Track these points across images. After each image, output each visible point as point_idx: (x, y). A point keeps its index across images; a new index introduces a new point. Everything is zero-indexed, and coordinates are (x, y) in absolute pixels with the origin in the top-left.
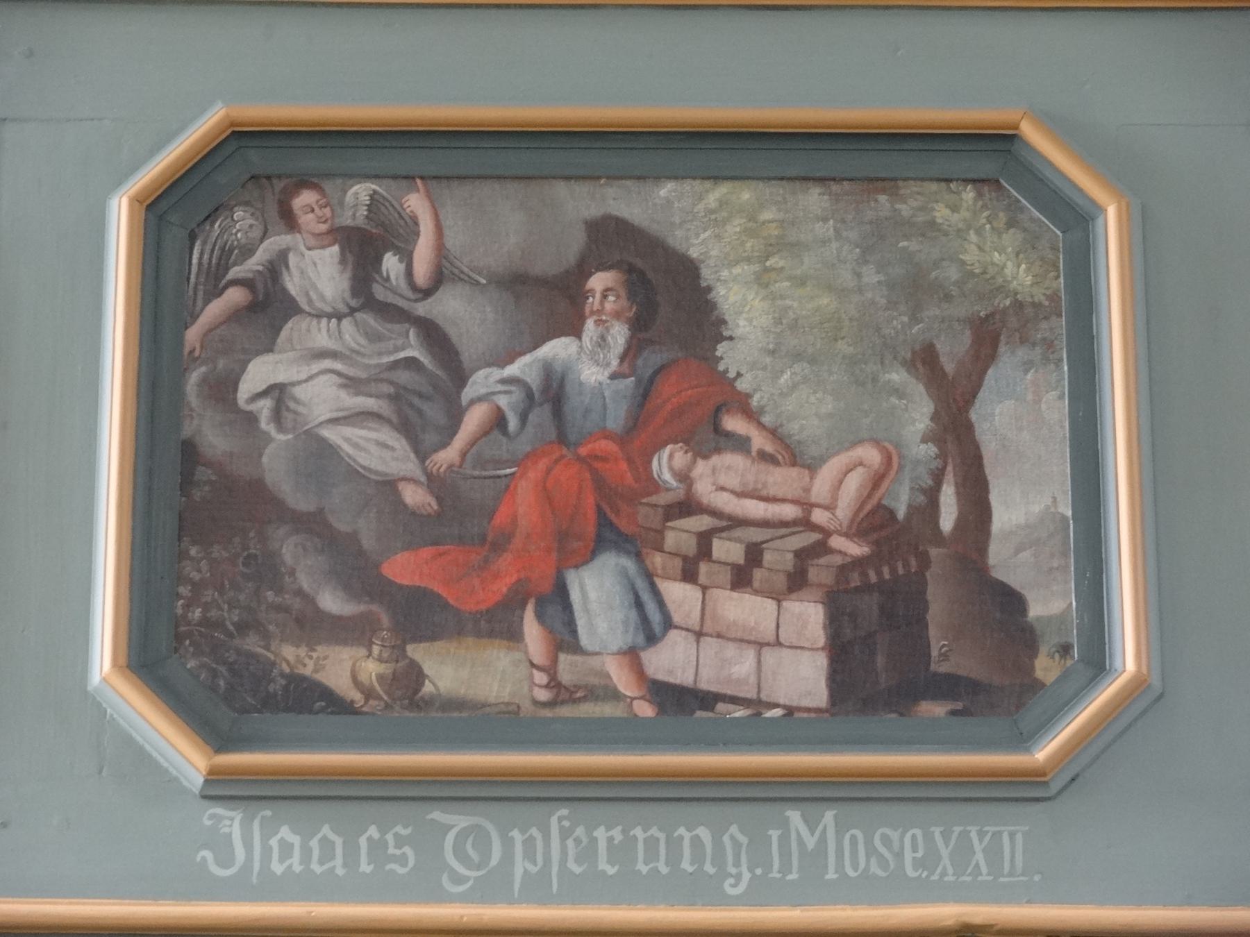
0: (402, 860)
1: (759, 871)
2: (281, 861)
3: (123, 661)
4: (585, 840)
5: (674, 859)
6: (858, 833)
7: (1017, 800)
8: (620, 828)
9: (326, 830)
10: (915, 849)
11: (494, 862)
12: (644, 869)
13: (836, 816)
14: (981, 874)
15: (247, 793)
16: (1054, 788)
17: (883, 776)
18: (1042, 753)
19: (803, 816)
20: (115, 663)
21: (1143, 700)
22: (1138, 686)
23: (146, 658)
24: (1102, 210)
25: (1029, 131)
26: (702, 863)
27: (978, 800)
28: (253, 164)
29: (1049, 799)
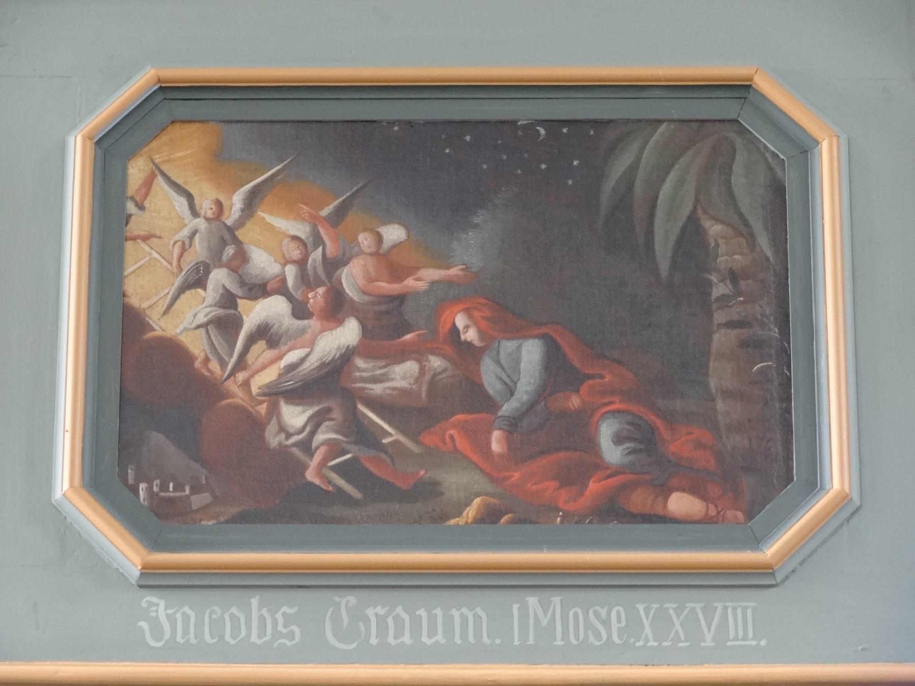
0: (291, 636)
6: (621, 609)
8: (702, 605)
10: (619, 621)
11: (363, 636)
13: (561, 601)
16: (779, 577)
17: (437, 568)
18: (770, 552)
19: (539, 601)
20: (72, 486)
21: (847, 511)
22: (843, 500)
24: (817, 143)
25: (762, 83)
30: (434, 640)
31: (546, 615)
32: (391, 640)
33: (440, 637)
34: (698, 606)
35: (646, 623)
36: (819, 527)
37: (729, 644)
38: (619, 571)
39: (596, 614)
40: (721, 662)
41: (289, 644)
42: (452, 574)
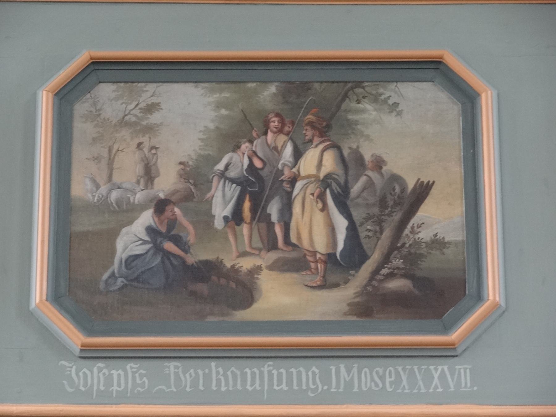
1: (326, 388)
2: (144, 382)
4: (193, 375)
7: (440, 356)
9: (314, 368)
10: (390, 377)
12: (250, 389)
14: (405, 389)
16: (459, 351)
18: (454, 336)
20: (479, 95)
23: (56, 297)
26: (228, 387)
28: (100, 69)
31: (436, 372)
33: (284, 387)
35: (419, 377)
37: (438, 390)
38: (433, 347)
39: (377, 373)
40: (396, 403)
41: (141, 390)
42: (352, 349)
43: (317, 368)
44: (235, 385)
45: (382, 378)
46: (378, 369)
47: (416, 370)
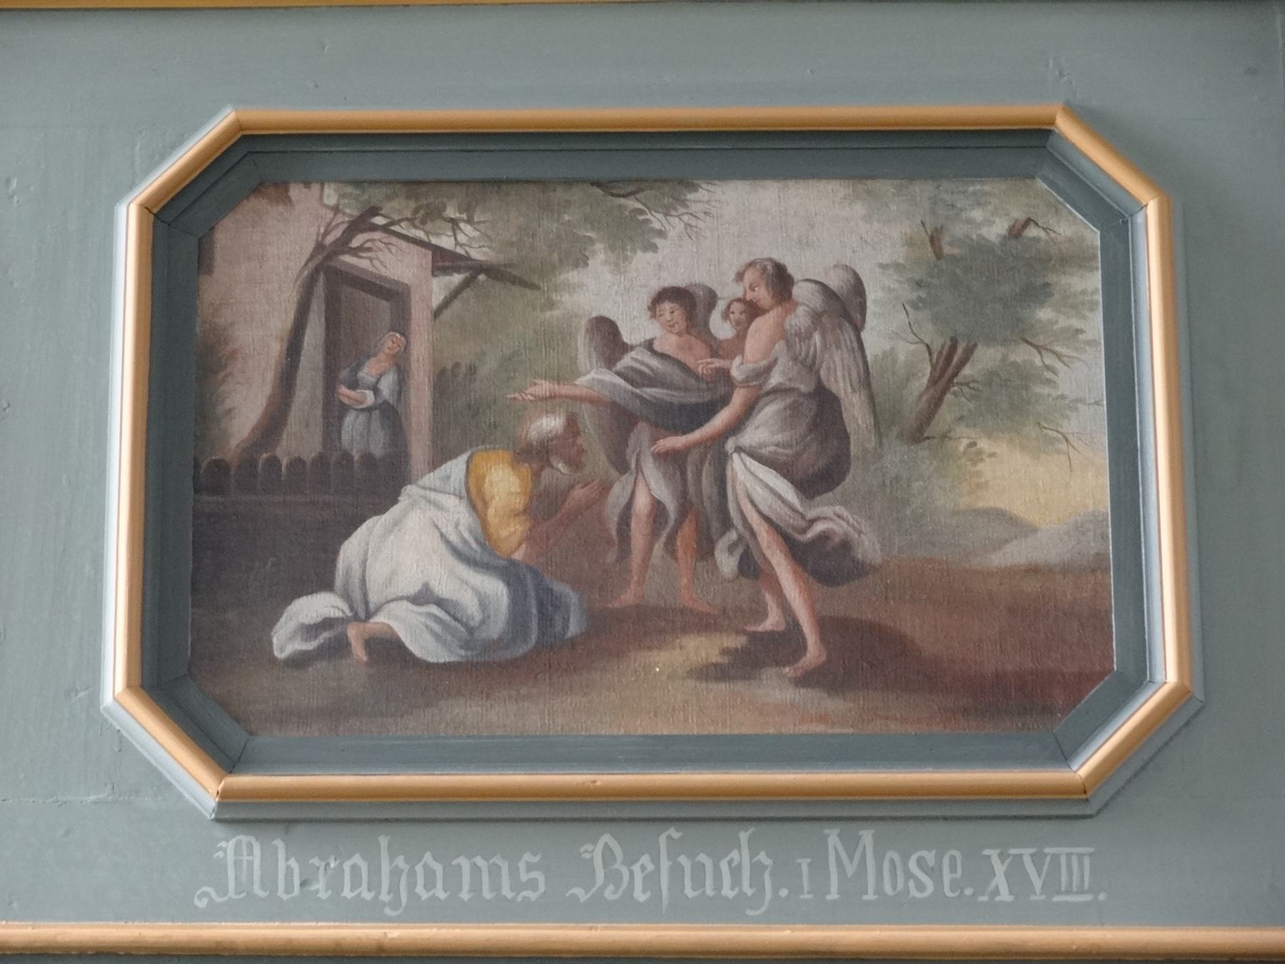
0: (532, 885)
2: (352, 890)
3: (137, 681)
5: (374, 885)
10: (953, 869)
15: (646, 816)
20: (129, 686)
22: (1179, 698)
24: (1143, 207)
25: (1066, 128)
26: (378, 894)
27: (936, 818)
28: (253, 163)
29: (1090, 816)
30: (431, 893)
31: (851, 859)
32: (347, 893)
34: (1026, 852)
36: (579, 799)
39: (921, 863)
43: (768, 855)
44: (496, 887)
45: (935, 873)
46: (924, 853)
47: (1027, 861)
